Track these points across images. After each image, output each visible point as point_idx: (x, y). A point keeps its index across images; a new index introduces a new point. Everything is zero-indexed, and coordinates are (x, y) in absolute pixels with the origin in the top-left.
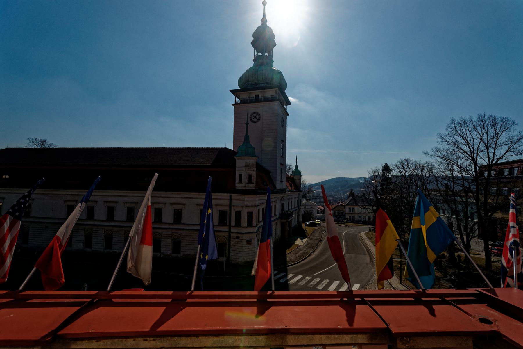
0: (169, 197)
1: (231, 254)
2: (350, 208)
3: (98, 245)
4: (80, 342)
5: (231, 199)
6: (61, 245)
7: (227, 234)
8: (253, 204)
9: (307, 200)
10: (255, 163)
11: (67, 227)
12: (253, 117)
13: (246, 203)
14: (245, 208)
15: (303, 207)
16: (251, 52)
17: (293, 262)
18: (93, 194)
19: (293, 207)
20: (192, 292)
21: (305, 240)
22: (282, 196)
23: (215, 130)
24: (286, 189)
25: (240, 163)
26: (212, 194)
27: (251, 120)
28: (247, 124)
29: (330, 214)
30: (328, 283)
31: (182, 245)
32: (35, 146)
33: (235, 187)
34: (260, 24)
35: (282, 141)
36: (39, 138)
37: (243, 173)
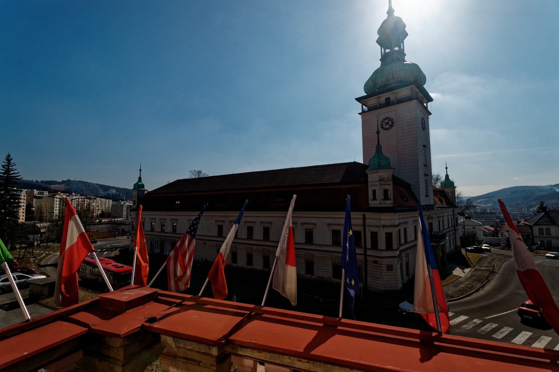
0: (300, 217)
1: (369, 280)
2: (541, 230)
3: (258, 265)
4: (244, 350)
5: (364, 219)
6: (223, 261)
7: (363, 257)
8: (392, 224)
9: (466, 218)
10: (391, 176)
11: (227, 245)
12: (384, 124)
13: (383, 222)
14: (382, 228)
15: (460, 227)
16: (377, 51)
17: (452, 297)
18: (244, 215)
19: (446, 227)
20: (340, 319)
21: (467, 270)
22: (429, 213)
23: (343, 143)
24: (435, 204)
25: (373, 177)
26: (351, 213)
27: (382, 127)
28: (378, 132)
29: (519, 239)
30: (511, 332)
31: (315, 267)
32: (194, 177)
33: (369, 204)
34: (385, 16)
35: (425, 146)
36: (196, 170)
37: (377, 188)
